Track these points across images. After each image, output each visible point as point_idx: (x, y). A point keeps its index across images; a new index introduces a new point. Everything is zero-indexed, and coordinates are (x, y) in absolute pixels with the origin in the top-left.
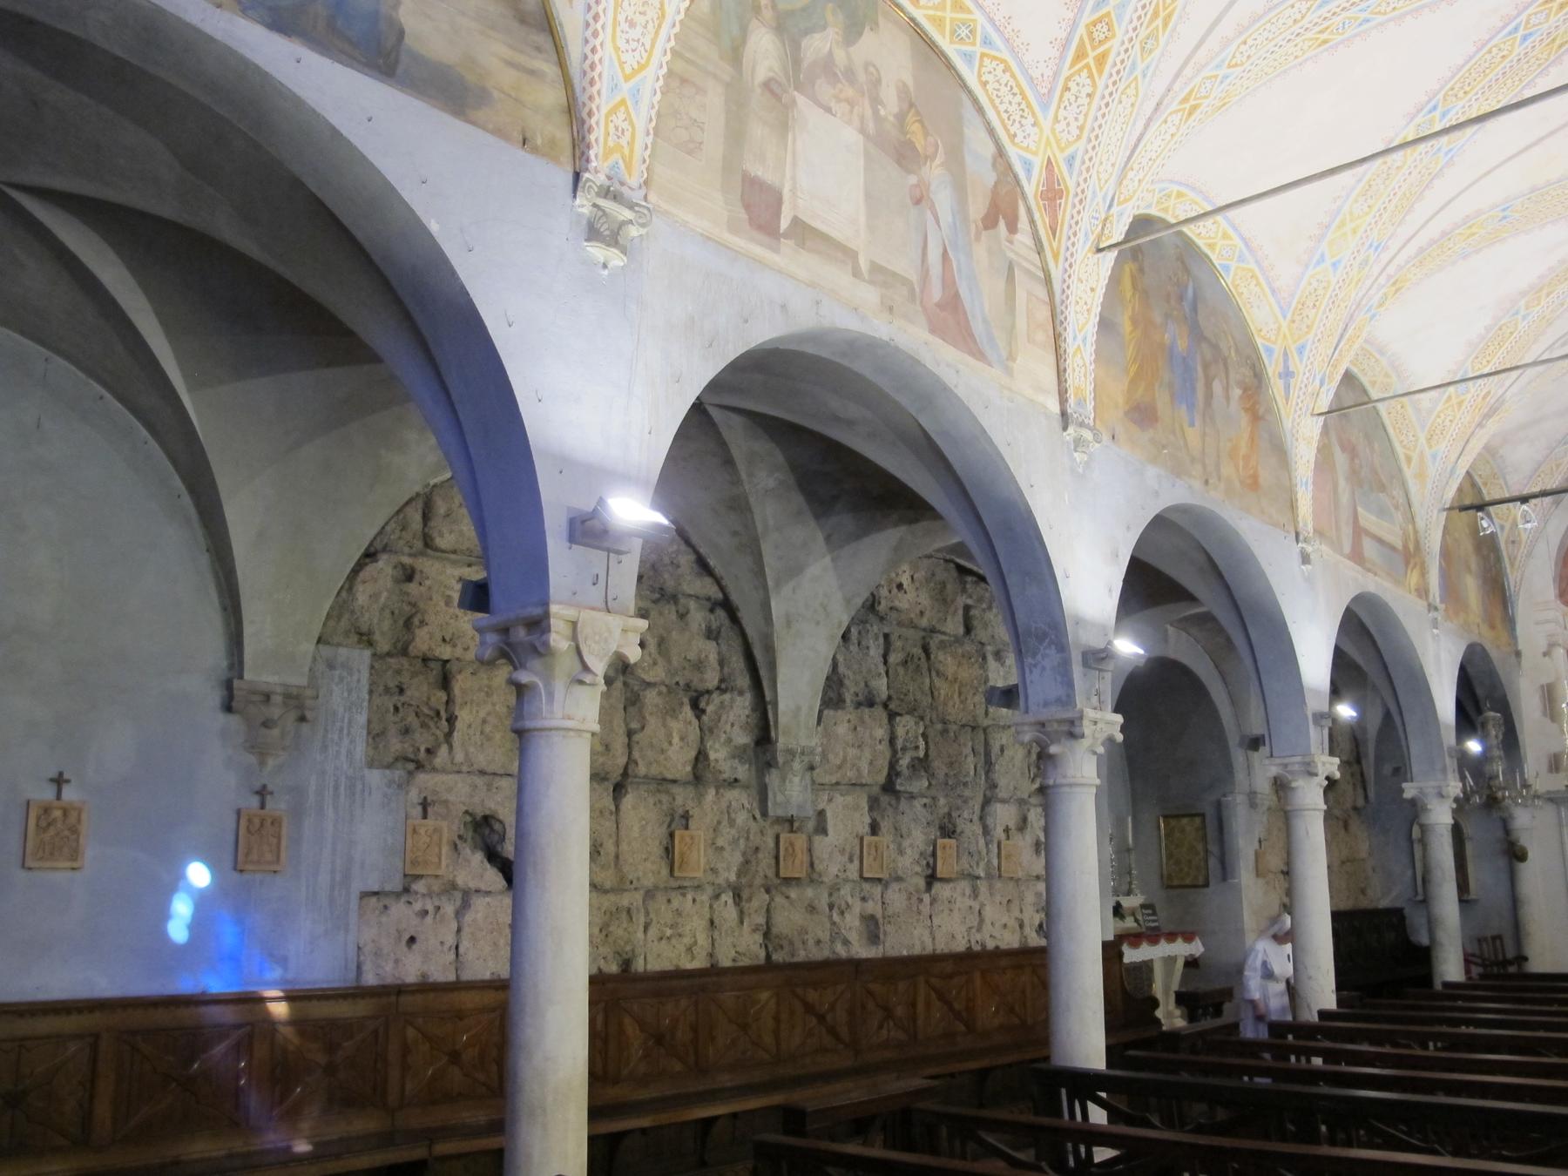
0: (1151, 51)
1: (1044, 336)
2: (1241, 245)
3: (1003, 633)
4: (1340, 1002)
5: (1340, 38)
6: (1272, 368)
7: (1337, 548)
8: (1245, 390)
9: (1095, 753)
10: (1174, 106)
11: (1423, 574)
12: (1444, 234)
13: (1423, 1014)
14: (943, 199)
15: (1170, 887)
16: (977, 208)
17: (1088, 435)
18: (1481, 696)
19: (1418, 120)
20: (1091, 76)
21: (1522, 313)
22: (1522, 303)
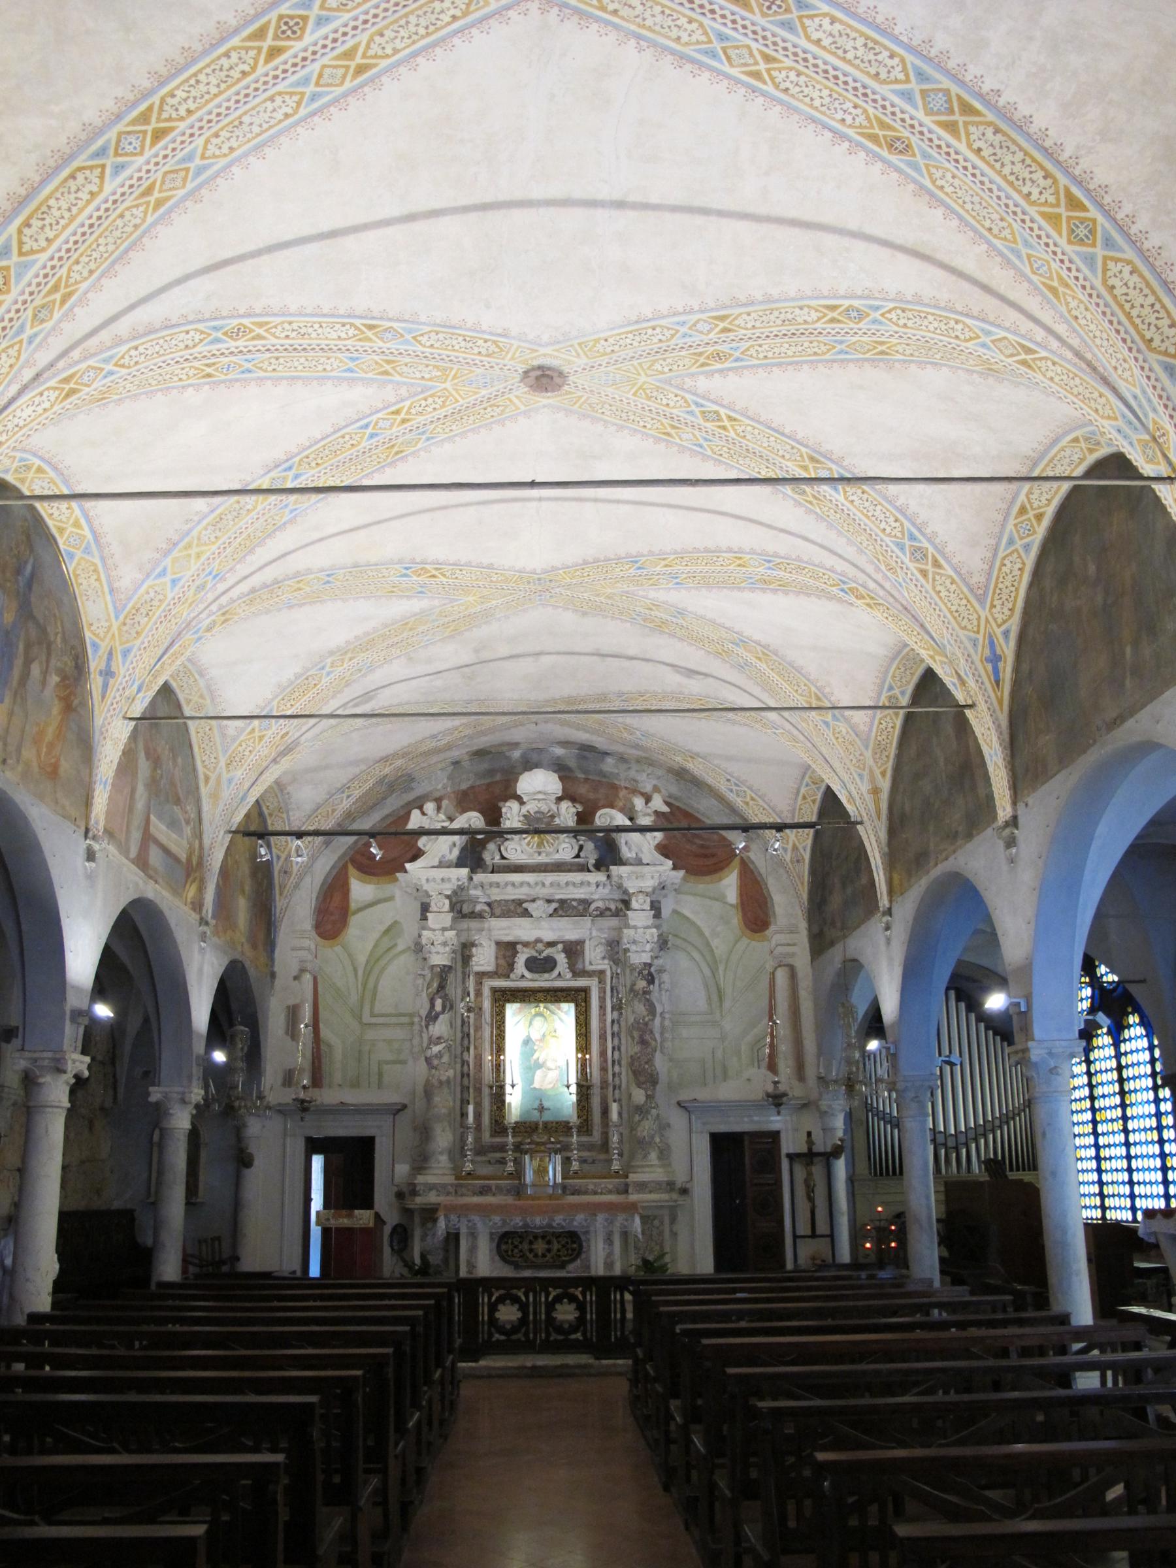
0: (43, 321)
2: (89, 536)
4: (54, 1305)
5: (223, 377)
6: (95, 664)
8: (64, 678)
10: (52, 383)
11: (201, 889)
12: (276, 582)
13: (156, 1313)
18: (235, 1008)
19: (273, 474)
21: (328, 669)
22: (329, 660)
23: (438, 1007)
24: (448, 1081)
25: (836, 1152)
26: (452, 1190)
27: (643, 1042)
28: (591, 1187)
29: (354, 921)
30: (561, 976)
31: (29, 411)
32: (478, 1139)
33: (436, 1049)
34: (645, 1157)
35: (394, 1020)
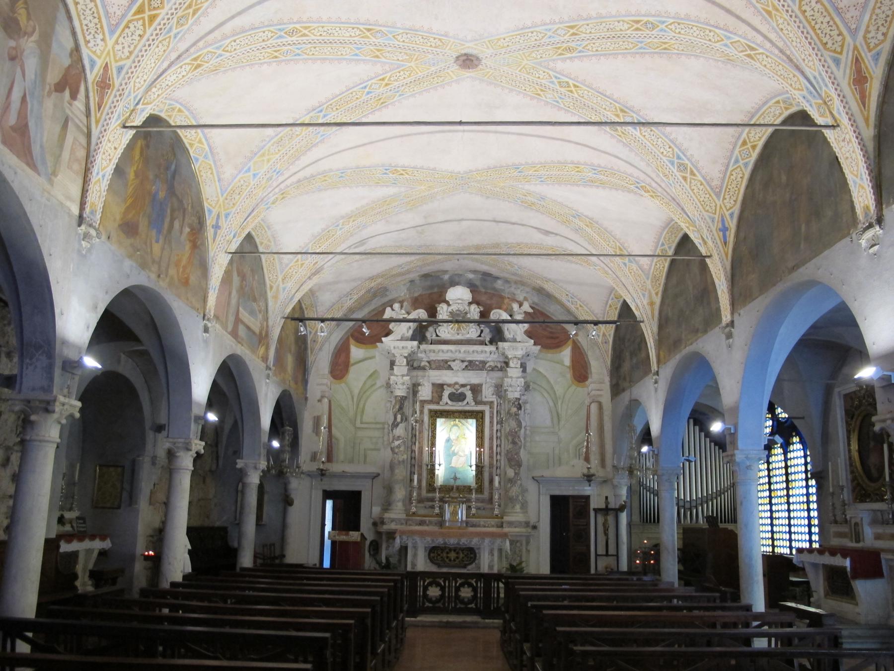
0: (182, 25)
1: (79, 167)
3: (14, 341)
6: (210, 221)
7: (225, 327)
8: (192, 230)
9: (59, 423)
10: (188, 61)
11: (267, 349)
12: (312, 176)
14: (31, 63)
15: (96, 507)
16: (53, 76)
17: (93, 232)
18: (285, 417)
19: (311, 114)
20: (144, 25)
23: (399, 419)
24: (403, 461)
25: (622, 508)
26: (404, 522)
27: (514, 443)
28: (482, 523)
29: (352, 369)
30: (469, 404)
31: (174, 77)
32: (419, 494)
33: (397, 443)
34: (513, 507)
35: (374, 426)
